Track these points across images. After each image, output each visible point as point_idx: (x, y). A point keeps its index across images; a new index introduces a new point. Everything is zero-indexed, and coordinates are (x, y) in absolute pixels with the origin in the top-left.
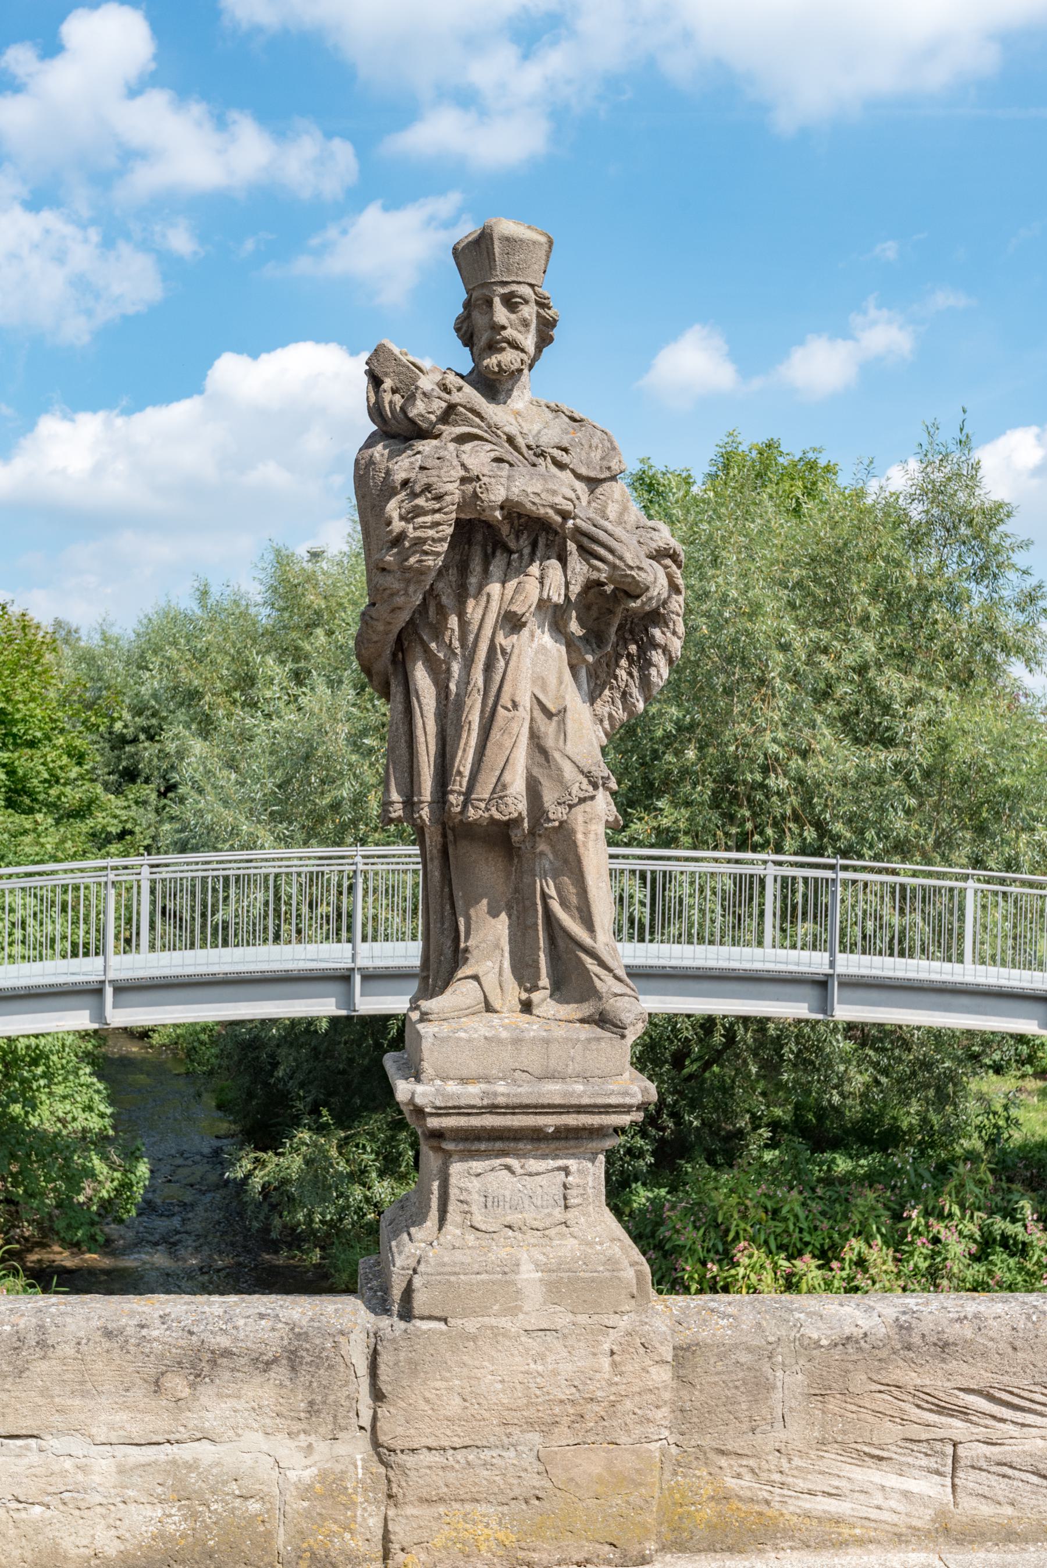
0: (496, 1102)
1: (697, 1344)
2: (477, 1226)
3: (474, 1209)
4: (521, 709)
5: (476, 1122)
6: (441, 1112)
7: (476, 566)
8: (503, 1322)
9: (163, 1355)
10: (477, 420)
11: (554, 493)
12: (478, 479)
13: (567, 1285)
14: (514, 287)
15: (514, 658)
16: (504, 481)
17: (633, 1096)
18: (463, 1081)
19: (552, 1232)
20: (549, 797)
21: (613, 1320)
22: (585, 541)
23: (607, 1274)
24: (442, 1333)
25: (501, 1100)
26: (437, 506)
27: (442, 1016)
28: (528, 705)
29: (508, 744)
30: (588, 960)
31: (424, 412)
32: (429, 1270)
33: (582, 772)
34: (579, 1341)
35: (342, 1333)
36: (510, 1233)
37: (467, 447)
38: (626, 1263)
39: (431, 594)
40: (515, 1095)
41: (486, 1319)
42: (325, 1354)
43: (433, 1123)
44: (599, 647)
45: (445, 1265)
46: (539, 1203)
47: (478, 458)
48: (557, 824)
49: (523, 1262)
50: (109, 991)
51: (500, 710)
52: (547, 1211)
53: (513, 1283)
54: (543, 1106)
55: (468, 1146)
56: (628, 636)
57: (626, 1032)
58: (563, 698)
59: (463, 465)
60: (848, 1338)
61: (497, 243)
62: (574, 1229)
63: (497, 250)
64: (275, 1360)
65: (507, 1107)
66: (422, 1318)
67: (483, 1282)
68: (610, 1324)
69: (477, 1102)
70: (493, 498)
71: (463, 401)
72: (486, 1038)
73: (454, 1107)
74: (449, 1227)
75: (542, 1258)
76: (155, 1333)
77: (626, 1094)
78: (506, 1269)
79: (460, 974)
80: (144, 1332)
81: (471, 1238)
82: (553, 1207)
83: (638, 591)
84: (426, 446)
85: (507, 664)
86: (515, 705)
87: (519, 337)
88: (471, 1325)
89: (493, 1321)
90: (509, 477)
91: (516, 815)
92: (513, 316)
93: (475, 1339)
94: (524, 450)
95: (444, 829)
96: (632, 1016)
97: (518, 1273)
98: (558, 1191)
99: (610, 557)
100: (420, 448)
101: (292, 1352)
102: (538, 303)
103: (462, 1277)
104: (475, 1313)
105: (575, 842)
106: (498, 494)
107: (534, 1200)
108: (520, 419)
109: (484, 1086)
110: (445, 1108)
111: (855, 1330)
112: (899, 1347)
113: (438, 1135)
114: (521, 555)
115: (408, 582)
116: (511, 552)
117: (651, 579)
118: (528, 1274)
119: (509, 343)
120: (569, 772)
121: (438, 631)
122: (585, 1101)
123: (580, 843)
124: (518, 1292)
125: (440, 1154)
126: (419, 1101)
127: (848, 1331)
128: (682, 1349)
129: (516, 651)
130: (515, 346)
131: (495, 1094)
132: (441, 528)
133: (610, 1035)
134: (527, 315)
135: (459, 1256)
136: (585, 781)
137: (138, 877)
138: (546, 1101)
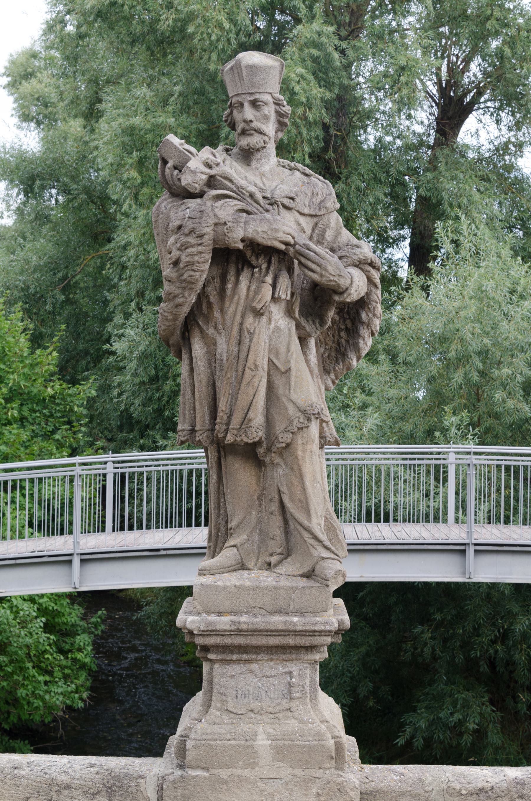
0: (240, 627)
1: (377, 791)
2: (231, 710)
3: (229, 699)
4: (260, 369)
5: (228, 641)
6: (205, 634)
7: (231, 277)
8: (246, 772)
9: (27, 786)
10: (229, 184)
11: (277, 230)
12: (225, 223)
13: (296, 752)
14: (257, 96)
15: (256, 336)
16: (242, 224)
17: (331, 625)
18: (220, 614)
19: (280, 715)
20: (279, 427)
21: (318, 773)
22: (302, 260)
23: (315, 743)
24: (205, 778)
25: (244, 627)
26: (200, 242)
27: (212, 572)
28: (266, 367)
29: (252, 392)
30: (306, 535)
31: (191, 182)
32: (197, 737)
33: (300, 410)
34: (296, 786)
35: (141, 777)
36: (253, 715)
37: (220, 203)
38: (329, 736)
39: (202, 296)
40: (253, 623)
41: (234, 770)
42: (130, 789)
43: (200, 641)
44: (321, 325)
45: (207, 734)
46: (272, 696)
47: (226, 210)
48: (284, 445)
49: (259, 733)
50: (76, 561)
51: (247, 370)
52: (277, 701)
53: (253, 747)
54: (271, 631)
55: (224, 656)
56: (346, 316)
57: (329, 583)
58: (289, 362)
59: (215, 215)
60: (480, 790)
61: (244, 70)
62: (296, 714)
63: (244, 74)
64: (99, 792)
65: (247, 631)
66: (193, 768)
67: (232, 746)
68: (317, 775)
69: (228, 627)
70: (235, 236)
71: (219, 173)
72: (235, 586)
73: (213, 631)
74: (212, 710)
75: (272, 731)
76: (23, 773)
77: (326, 623)
78: (248, 738)
79: (227, 545)
80: (16, 771)
81: (226, 718)
82: (282, 699)
83: (341, 290)
84: (193, 203)
85: (251, 340)
86: (256, 366)
87: (263, 127)
88: (224, 774)
89: (239, 772)
90: (246, 222)
91: (257, 439)
92: (258, 114)
93: (226, 782)
94: (261, 201)
95: (219, 447)
96: (333, 573)
97: (255, 741)
98: (283, 688)
99: (318, 269)
100: (189, 205)
101: (109, 788)
102: (275, 103)
103: (218, 742)
104: (227, 766)
105: (297, 457)
106: (239, 233)
107: (269, 694)
108: (264, 179)
109: (233, 618)
110: (207, 631)
111: (485, 784)
112: (515, 796)
113: (206, 649)
114: (261, 269)
115: (184, 288)
116: (254, 267)
117: (348, 282)
118: (262, 742)
119: (255, 130)
120: (291, 410)
121: (208, 318)
122: (299, 628)
123: (300, 458)
124: (256, 753)
125: (208, 663)
126: (188, 626)
127: (480, 786)
128: (367, 794)
129: (257, 332)
130: (260, 132)
131: (240, 623)
132: (203, 255)
133: (318, 585)
134: (267, 113)
135: (217, 729)
136: (302, 417)
137: (104, 471)
138: (273, 628)
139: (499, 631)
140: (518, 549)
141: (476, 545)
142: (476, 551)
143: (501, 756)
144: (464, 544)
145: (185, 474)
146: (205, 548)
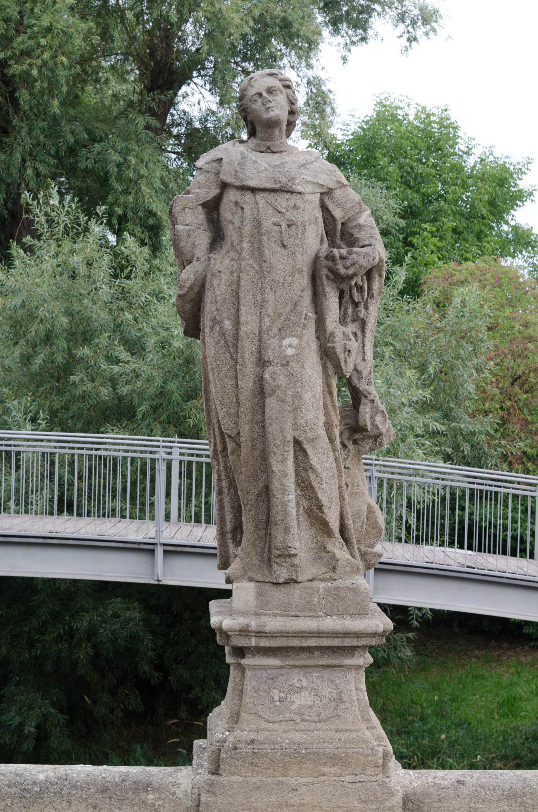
50: (159, 551)
139: (64, 628)
140: (56, 541)
141: (165, 545)
142: (165, 552)
143: (169, 764)
144: (153, 544)
145: (144, 464)
146: (215, 548)
